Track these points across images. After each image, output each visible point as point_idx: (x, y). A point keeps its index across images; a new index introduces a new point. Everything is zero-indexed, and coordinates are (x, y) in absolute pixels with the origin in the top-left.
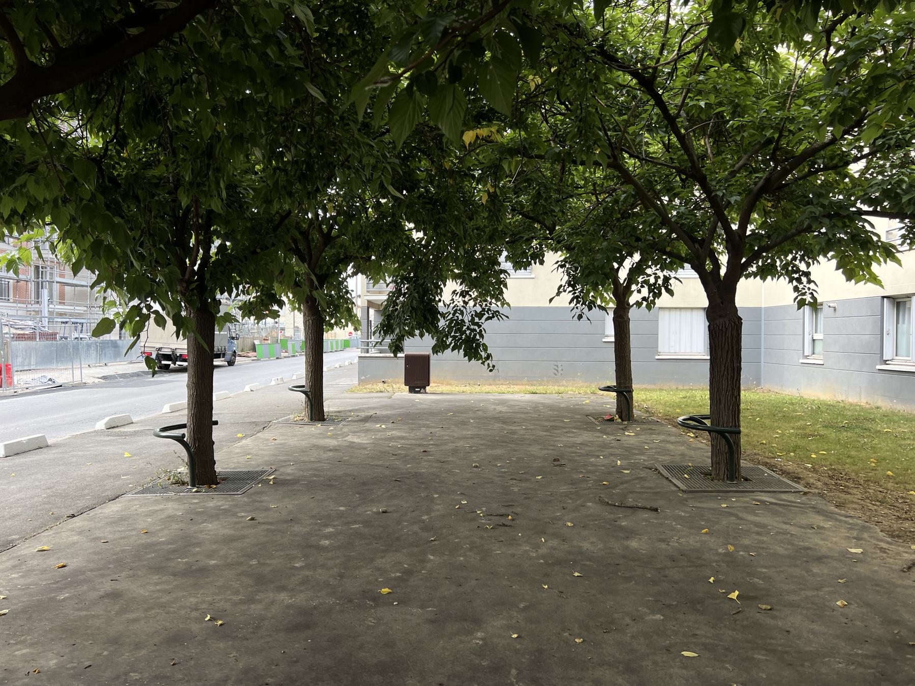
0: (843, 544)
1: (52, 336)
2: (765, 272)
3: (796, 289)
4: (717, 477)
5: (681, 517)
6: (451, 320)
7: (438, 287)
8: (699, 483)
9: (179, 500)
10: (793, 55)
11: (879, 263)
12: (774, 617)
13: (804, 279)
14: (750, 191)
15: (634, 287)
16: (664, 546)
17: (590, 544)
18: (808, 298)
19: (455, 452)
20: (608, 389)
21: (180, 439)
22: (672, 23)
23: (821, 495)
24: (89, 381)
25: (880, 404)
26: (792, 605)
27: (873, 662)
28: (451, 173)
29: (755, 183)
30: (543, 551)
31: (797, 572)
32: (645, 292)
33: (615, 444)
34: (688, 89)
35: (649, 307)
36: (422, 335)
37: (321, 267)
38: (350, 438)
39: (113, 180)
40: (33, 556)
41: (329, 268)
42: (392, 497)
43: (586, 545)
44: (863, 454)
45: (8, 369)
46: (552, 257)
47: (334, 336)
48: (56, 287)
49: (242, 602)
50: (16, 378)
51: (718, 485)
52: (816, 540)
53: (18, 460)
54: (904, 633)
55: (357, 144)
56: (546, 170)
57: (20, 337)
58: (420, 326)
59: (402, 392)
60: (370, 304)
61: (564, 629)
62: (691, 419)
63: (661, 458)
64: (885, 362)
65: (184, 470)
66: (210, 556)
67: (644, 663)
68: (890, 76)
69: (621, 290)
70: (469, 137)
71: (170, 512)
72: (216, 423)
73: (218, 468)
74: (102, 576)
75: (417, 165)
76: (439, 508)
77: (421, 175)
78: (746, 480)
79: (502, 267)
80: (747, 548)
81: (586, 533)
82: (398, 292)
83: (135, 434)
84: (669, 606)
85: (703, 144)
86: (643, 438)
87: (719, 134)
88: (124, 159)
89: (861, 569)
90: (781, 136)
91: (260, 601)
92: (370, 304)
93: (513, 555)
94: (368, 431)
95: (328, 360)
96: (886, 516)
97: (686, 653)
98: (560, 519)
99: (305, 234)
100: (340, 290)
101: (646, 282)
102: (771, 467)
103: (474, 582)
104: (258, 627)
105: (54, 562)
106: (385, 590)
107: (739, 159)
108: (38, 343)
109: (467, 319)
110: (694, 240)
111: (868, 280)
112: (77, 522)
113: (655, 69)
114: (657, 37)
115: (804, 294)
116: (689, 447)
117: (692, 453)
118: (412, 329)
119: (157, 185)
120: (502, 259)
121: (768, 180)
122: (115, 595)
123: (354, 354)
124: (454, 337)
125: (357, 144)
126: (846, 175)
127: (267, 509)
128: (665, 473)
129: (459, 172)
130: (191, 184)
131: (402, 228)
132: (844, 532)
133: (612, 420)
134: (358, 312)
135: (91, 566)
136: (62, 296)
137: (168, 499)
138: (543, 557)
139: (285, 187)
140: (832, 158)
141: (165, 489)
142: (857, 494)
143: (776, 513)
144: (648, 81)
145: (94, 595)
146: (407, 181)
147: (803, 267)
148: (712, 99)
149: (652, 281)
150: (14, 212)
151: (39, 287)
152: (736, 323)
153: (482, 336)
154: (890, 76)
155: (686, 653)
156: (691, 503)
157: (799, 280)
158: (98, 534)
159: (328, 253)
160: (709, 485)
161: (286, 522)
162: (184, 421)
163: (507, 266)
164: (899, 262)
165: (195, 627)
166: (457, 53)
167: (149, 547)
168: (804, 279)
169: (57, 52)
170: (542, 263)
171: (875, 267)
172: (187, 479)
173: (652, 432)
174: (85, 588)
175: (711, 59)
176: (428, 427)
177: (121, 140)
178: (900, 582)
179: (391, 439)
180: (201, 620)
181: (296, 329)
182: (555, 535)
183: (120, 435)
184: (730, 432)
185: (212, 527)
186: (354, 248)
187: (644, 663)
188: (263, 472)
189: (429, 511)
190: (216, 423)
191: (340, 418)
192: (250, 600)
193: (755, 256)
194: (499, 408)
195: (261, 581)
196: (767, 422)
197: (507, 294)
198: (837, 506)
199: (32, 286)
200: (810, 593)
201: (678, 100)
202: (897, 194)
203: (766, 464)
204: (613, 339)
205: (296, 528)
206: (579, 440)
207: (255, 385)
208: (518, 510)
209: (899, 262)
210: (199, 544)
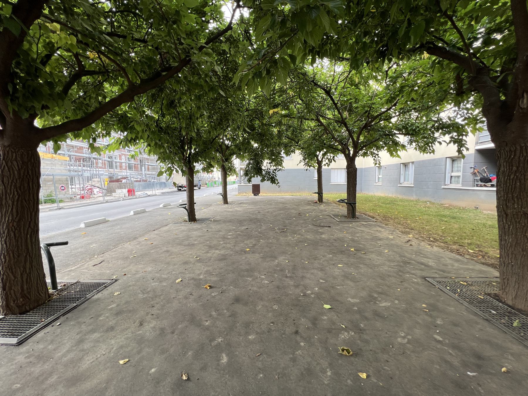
0: (387, 235)
1: (146, 181)
2: (365, 155)
3: (374, 159)
4: (349, 217)
5: (338, 229)
6: (266, 172)
7: (262, 162)
8: (343, 219)
9: (185, 226)
10: (374, 84)
11: (400, 151)
12: (366, 255)
13: (377, 156)
14: (360, 128)
15: (324, 160)
16: (332, 237)
17: (310, 236)
18: (378, 162)
19: (268, 212)
20: (315, 193)
21: (185, 208)
22: (335, 74)
23: (381, 222)
24: (158, 194)
25: (399, 196)
26: (372, 252)
27: (396, 267)
28: (266, 125)
29: (362, 125)
30: (296, 238)
31: (373, 243)
32: (327, 161)
33: (317, 209)
34: (341, 94)
35: (328, 166)
36: (257, 177)
37: (226, 157)
38: (236, 209)
39: (161, 128)
40: (143, 241)
41: (228, 157)
42: (249, 224)
43: (308, 237)
44: (394, 211)
45: (134, 191)
46: (298, 152)
47: (231, 179)
48: (146, 166)
49: (205, 253)
50: (136, 193)
51: (349, 220)
52: (378, 234)
53: (138, 216)
54: (406, 259)
55: (236, 114)
56: (296, 122)
57: (137, 181)
58: (257, 174)
59: (252, 195)
60: (241, 169)
61: (302, 259)
62: (341, 200)
63: (331, 213)
64: (401, 184)
65: (187, 218)
66: (195, 241)
67: (326, 268)
68: (407, 86)
69: (319, 162)
70: (271, 112)
71: (183, 229)
72: (195, 203)
73: (197, 217)
74: (164, 246)
75: (255, 122)
76: (264, 227)
77: (256, 126)
78: (358, 218)
79: (282, 156)
80: (358, 237)
81: (308, 233)
82: (249, 164)
83: (172, 208)
84: (334, 253)
85: (346, 114)
86: (326, 207)
87: (350, 111)
88: (164, 121)
89: (392, 242)
90: (370, 109)
91: (210, 253)
92: (241, 169)
93: (286, 240)
94: (241, 207)
95: (228, 187)
96: (400, 227)
97: (339, 265)
98: (301, 230)
99: (220, 146)
100: (232, 164)
101: (327, 158)
102: (365, 215)
103: (275, 247)
104: (210, 260)
105: (149, 243)
106: (248, 249)
107: (357, 117)
108: (142, 183)
109: (271, 171)
110: (342, 144)
111: (396, 157)
112: (156, 232)
113: (330, 87)
114: (331, 79)
115: (377, 161)
116: (340, 210)
117: (341, 211)
118: (254, 175)
119: (174, 129)
120: (282, 153)
121: (366, 124)
122: (167, 251)
123: (236, 186)
124: (267, 177)
125: (236, 114)
126: (391, 123)
127: (211, 228)
128: (333, 217)
129: (268, 125)
130: (185, 128)
131: (251, 143)
132: (387, 232)
133: (316, 202)
134: (237, 170)
135: (160, 243)
136: (148, 169)
137: (182, 226)
138: (296, 240)
139: (214, 127)
140: (386, 117)
141: (181, 223)
142: (392, 221)
143: (367, 227)
144: (328, 92)
145: (161, 251)
146: (252, 128)
147: (376, 152)
148: (349, 97)
149: (329, 158)
150: (132, 139)
151: (141, 166)
152: (356, 170)
153: (276, 176)
154: (407, 86)
155: (339, 265)
156: (341, 225)
157: (375, 157)
158: (162, 235)
159: (228, 152)
160: (346, 220)
161: (217, 231)
162: (186, 203)
163: (284, 155)
164: (406, 151)
165: (191, 260)
166: (268, 65)
167: (177, 238)
168: (377, 156)
169: (142, 80)
170: (295, 153)
171: (399, 152)
172: (188, 220)
173: (329, 205)
174: (159, 249)
175: (348, 85)
176: (259, 205)
177: (163, 116)
178: (405, 245)
179: (248, 209)
180: (193, 258)
181: (219, 178)
182: (299, 234)
183: (167, 208)
184: (353, 204)
185: (195, 233)
186: (236, 150)
187: (326, 268)
188: (210, 218)
189: (261, 228)
190: (195, 203)
191: (232, 203)
192: (207, 252)
193: (361, 149)
194: (282, 200)
195: (210, 247)
196: (364, 202)
197: (284, 164)
198: (386, 225)
199: (139, 166)
200: (377, 249)
201: (338, 99)
202: (407, 127)
203: (364, 214)
204: (317, 179)
205: (220, 233)
206: (306, 208)
207: (207, 194)
208: (288, 228)
209: (406, 151)
210: (191, 238)
